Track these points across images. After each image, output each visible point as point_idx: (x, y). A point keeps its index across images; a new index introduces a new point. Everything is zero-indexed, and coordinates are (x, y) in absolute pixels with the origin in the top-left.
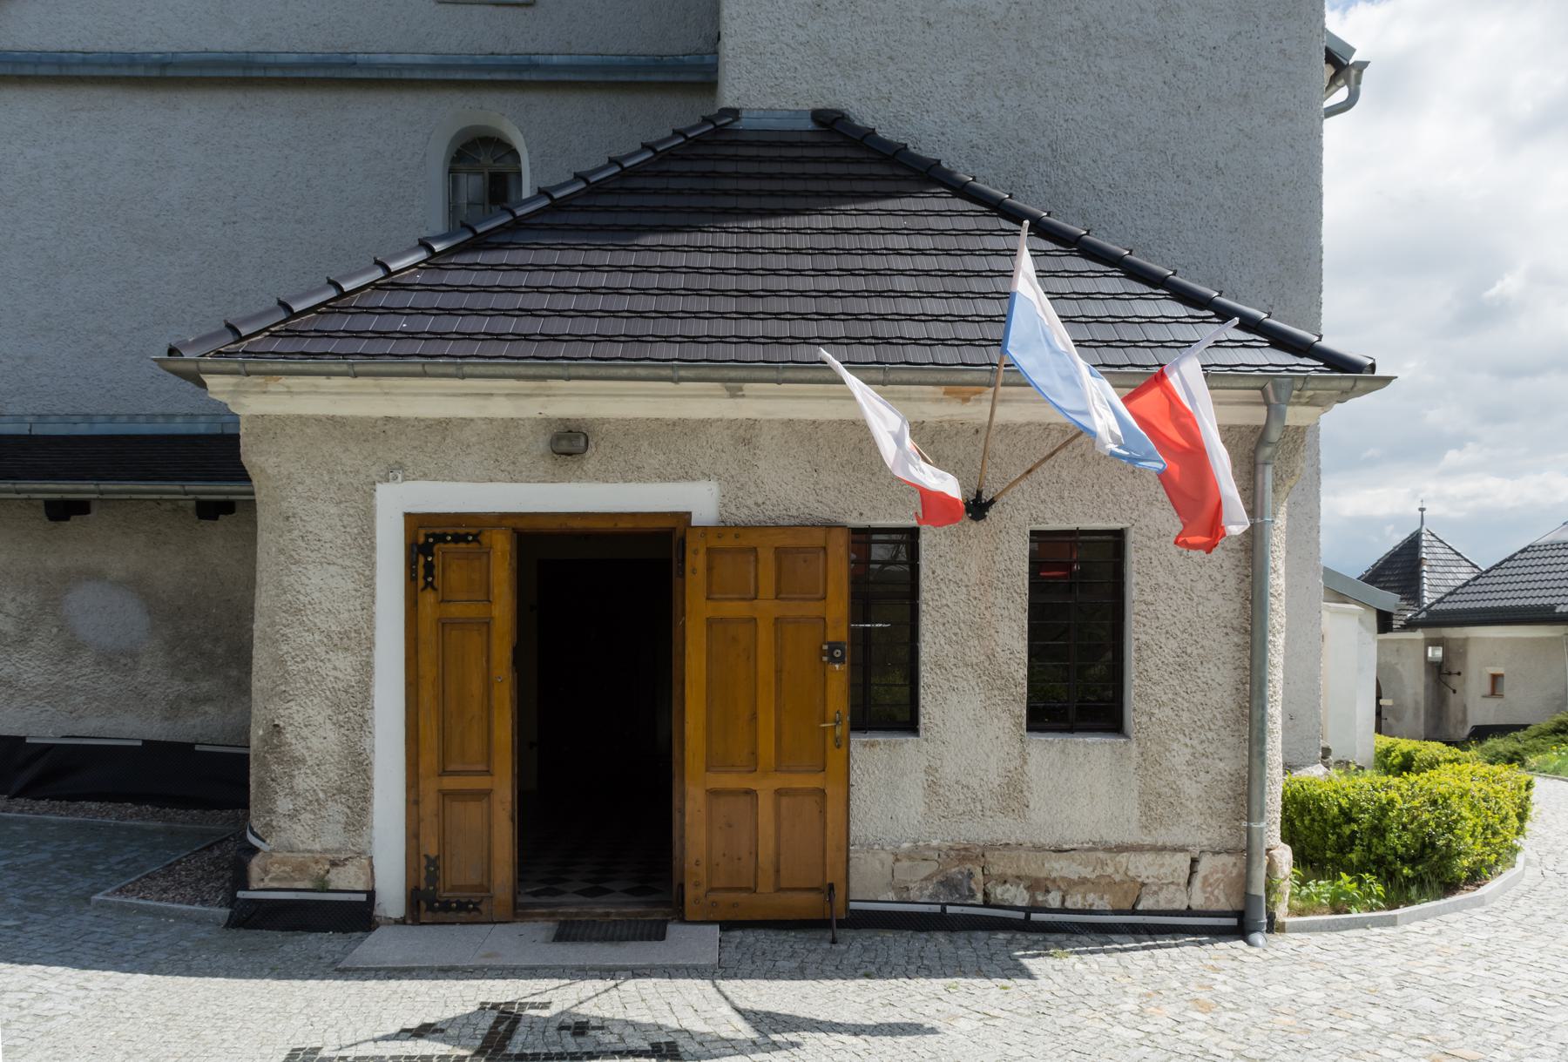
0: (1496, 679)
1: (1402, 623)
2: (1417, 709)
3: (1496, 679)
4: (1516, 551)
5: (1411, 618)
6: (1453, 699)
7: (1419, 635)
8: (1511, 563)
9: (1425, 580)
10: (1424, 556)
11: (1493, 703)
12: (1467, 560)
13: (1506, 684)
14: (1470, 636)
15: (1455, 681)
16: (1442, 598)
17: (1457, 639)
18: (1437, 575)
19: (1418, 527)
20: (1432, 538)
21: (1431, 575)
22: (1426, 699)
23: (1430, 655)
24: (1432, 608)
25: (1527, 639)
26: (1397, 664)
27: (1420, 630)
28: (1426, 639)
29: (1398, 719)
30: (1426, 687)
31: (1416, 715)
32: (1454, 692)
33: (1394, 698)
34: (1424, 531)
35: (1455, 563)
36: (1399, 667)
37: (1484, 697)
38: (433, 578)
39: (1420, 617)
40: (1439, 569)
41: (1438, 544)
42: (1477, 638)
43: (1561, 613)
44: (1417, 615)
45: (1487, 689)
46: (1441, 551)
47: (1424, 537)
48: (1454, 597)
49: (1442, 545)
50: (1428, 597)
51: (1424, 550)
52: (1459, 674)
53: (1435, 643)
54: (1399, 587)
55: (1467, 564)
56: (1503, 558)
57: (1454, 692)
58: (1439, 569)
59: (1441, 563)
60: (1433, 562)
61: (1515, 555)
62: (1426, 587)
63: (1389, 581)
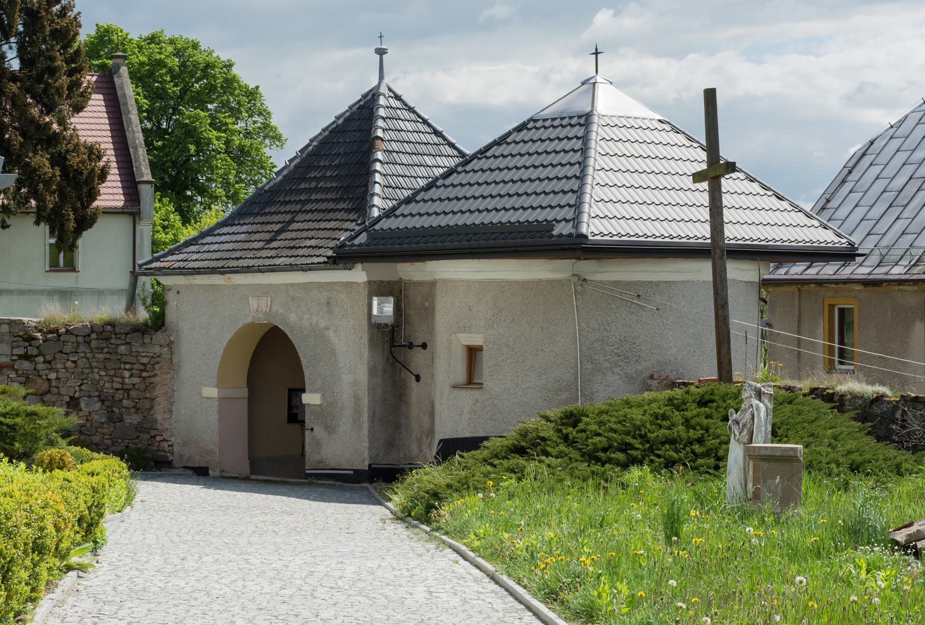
0: (473, 352)
1: (330, 253)
2: (357, 411)
3: (473, 352)
4: (510, 127)
5: (343, 245)
6: (415, 391)
7: (358, 275)
8: (503, 149)
9: (378, 177)
10: (380, 133)
11: (467, 397)
12: (452, 145)
13: (487, 361)
14: (437, 278)
15: (418, 358)
16: (394, 209)
17: (420, 284)
18: (400, 170)
19: (374, 82)
20: (394, 103)
21: (389, 169)
22: (372, 390)
23: (375, 312)
24: (377, 227)
25: (517, 282)
26: (327, 328)
27: (359, 266)
28: (369, 282)
29: (330, 430)
30: (372, 372)
31: (356, 421)
32: (418, 378)
33: (323, 392)
34: (383, 89)
35: (431, 150)
36: (331, 334)
37: (454, 387)
38: (678, 537)
39: (356, 241)
40: (404, 159)
41: (406, 114)
42: (444, 280)
43: (561, 235)
44: (352, 238)
45: (460, 373)
46: (410, 126)
47: (382, 101)
48: (412, 208)
49: (413, 116)
50: (379, 203)
51: (380, 123)
52: (424, 346)
53: (380, 289)
54: (337, 189)
55: (450, 151)
56: (490, 140)
57: (418, 378)
58: (404, 159)
59: (408, 148)
60: (395, 146)
61: (509, 134)
62: (377, 189)
63: (324, 178)
